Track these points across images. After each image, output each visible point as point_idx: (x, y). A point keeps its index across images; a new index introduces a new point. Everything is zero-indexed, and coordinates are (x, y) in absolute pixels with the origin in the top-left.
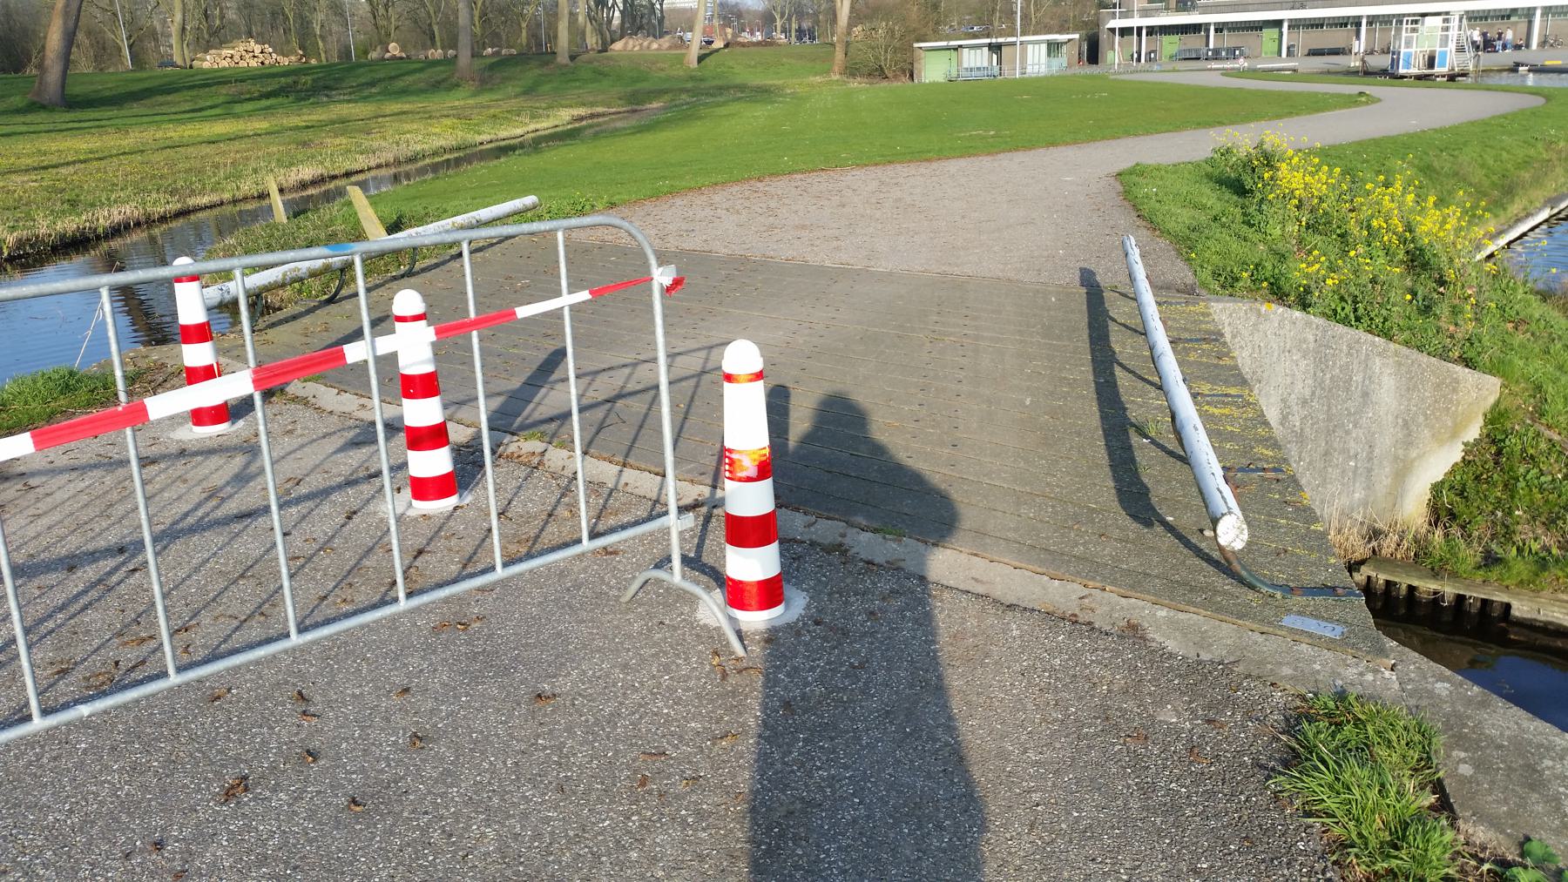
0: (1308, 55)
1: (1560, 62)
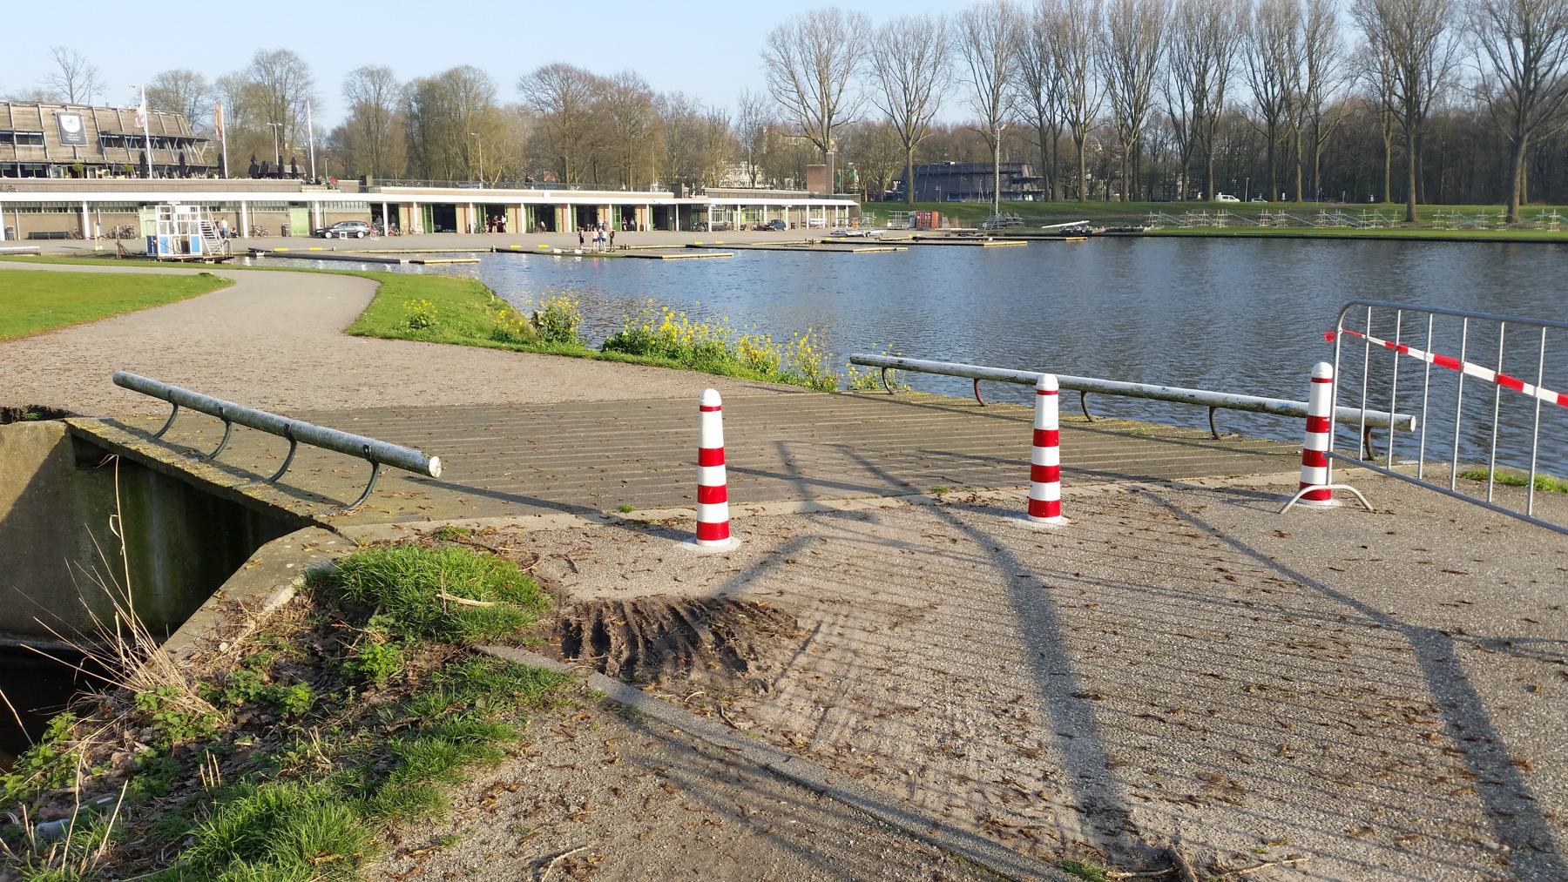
0: (30, 238)
1: (286, 249)
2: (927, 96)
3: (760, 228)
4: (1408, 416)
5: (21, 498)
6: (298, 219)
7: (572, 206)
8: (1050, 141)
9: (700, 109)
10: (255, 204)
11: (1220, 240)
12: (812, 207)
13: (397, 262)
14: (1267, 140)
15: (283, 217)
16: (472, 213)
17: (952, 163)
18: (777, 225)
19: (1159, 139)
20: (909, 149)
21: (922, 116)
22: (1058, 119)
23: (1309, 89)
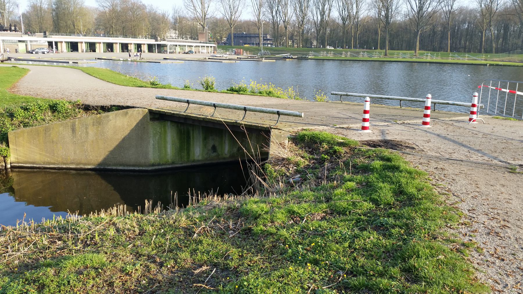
2: (237, 10)
3: (185, 53)
4: (482, 105)
5: (133, 129)
6: (22, 47)
7: (119, 43)
8: (276, 27)
9: (159, 10)
10: (5, 41)
11: (331, 61)
12: (202, 46)
13: (68, 63)
14: (342, 29)
15: (16, 46)
16: (84, 45)
17: (244, 33)
18: (190, 52)
19: (309, 28)
20: (231, 28)
21: (236, 17)
22: (279, 20)
23: (356, 13)
